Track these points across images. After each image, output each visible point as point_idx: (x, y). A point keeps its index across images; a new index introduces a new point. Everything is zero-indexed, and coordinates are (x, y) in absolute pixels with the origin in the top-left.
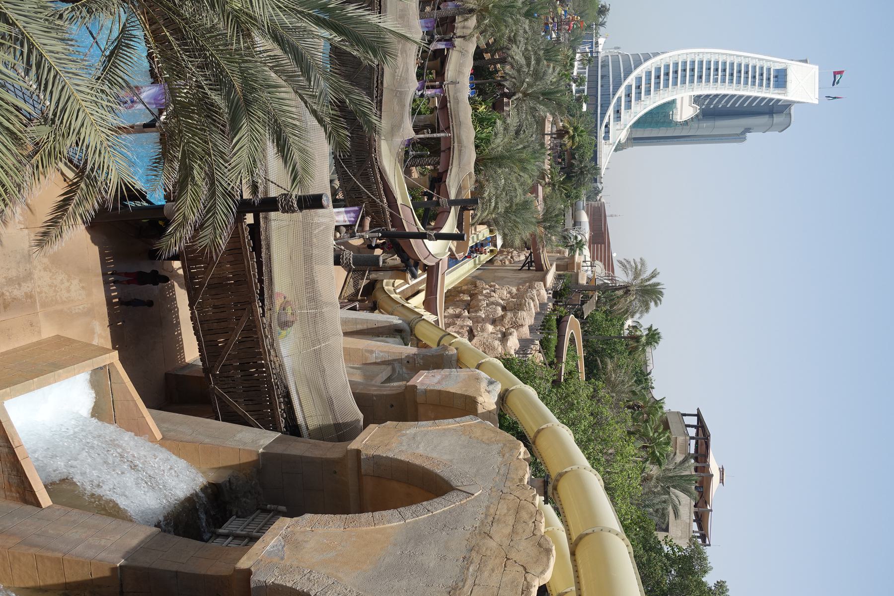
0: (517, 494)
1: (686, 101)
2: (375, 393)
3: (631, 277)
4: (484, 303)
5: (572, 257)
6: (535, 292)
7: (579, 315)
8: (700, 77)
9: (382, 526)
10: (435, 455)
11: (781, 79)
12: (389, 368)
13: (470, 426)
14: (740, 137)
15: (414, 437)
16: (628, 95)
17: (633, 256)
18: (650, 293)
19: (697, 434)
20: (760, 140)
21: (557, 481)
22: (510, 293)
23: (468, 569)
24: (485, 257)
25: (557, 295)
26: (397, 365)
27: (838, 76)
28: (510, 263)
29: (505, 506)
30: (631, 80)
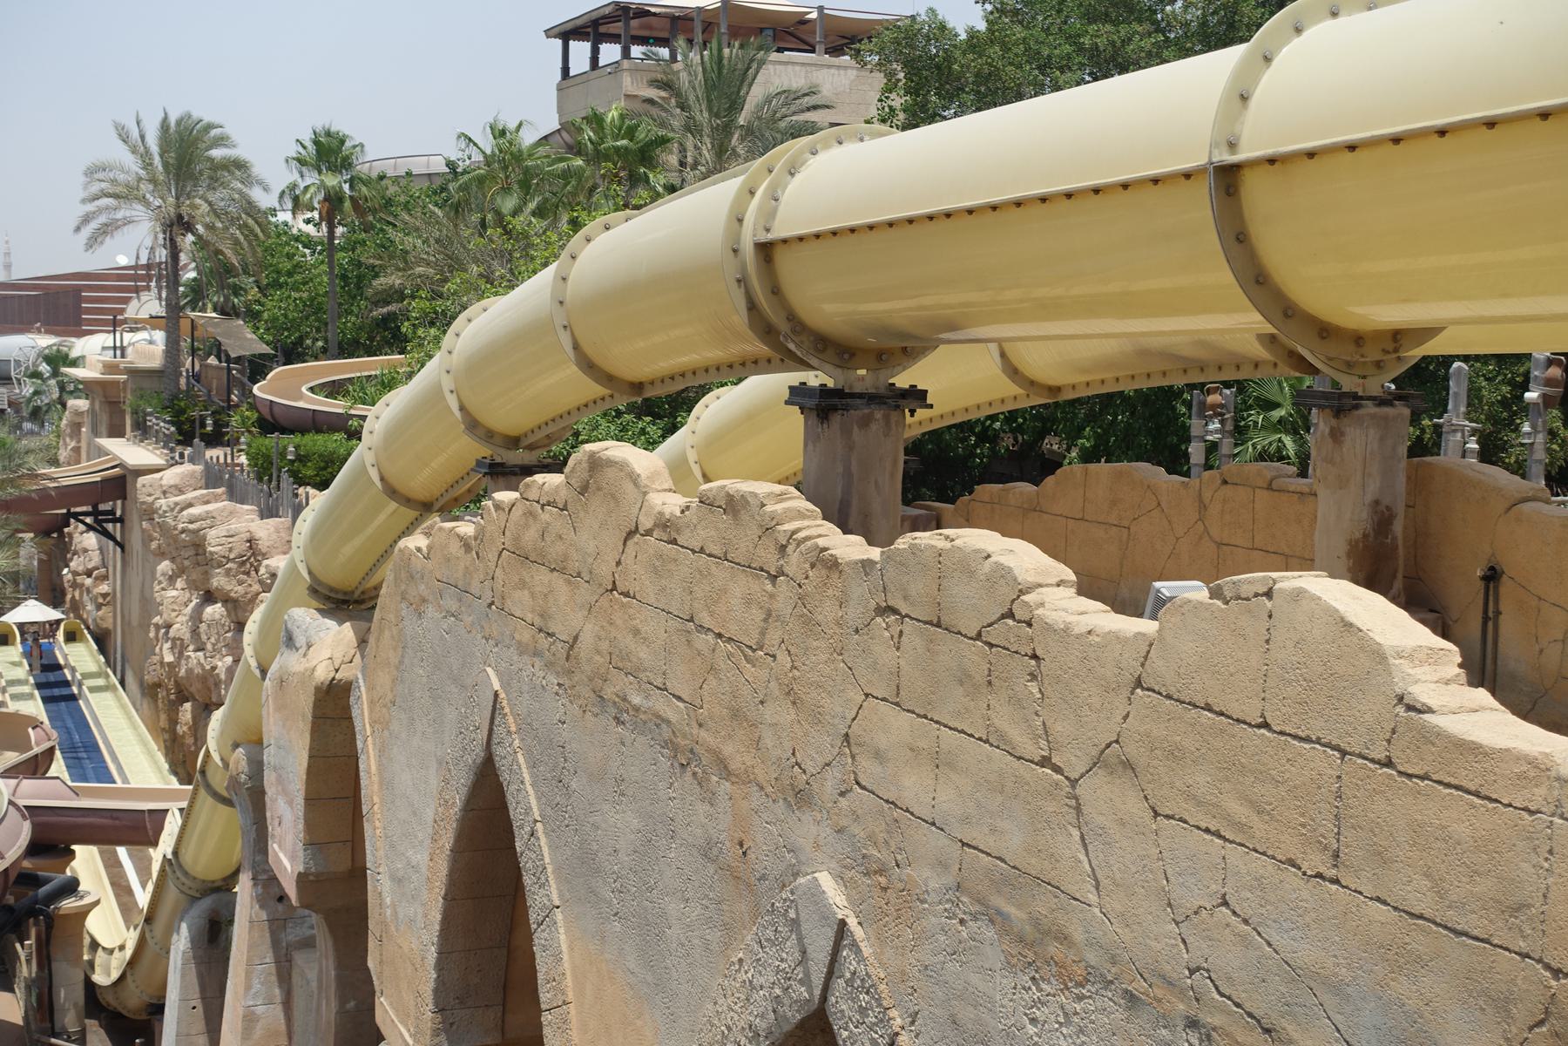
0: (492, 556)
2: (334, 1005)
3: (138, 211)
4: (194, 657)
5: (87, 388)
6: (163, 503)
7: (257, 368)
9: (569, 981)
10: (429, 814)
12: (299, 958)
13: (372, 702)
15: (398, 881)
17: (70, 199)
18: (187, 156)
19: (614, 38)
21: (489, 436)
22: (172, 580)
23: (637, 709)
24: (80, 658)
25: (189, 431)
26: (292, 935)
28: (105, 578)
29: (518, 594)
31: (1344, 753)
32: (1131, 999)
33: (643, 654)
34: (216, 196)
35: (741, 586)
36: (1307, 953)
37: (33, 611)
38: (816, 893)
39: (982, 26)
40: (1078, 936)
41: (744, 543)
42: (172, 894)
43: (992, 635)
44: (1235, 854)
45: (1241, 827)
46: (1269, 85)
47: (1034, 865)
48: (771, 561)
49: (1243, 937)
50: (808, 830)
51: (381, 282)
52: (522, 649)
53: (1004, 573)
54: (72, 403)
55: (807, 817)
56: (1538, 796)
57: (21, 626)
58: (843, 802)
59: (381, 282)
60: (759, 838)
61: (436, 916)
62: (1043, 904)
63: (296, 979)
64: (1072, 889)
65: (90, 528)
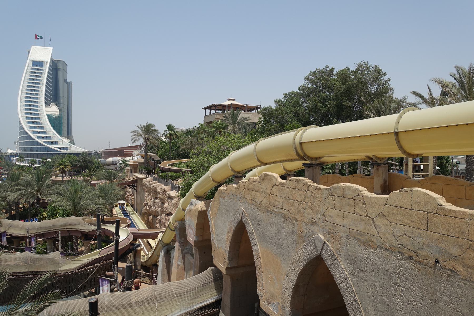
0: (242, 190)
1: (48, 109)
3: (140, 137)
4: (154, 208)
7: (160, 162)
8: (35, 102)
10: (226, 230)
11: (38, 64)
12: (186, 255)
14: (69, 85)
16: (43, 138)
19: (213, 109)
20: (71, 75)
22: (148, 196)
24: (129, 209)
25: (149, 172)
27: (38, 37)
30: (34, 136)
31: (428, 212)
32: (387, 250)
33: (277, 203)
34: (153, 135)
35: (299, 193)
36: (422, 241)
37: (122, 202)
38: (319, 238)
39: (274, 108)
40: (375, 241)
41: (300, 186)
42: (160, 245)
43: (355, 198)
44: (406, 228)
45: (408, 224)
46: (401, 121)
47: (365, 231)
48: (306, 189)
49: (409, 239)
50: (315, 228)
51: (181, 148)
52: (249, 204)
53: (358, 189)
54: (127, 168)
55: (315, 226)
56: (466, 217)
57: (119, 204)
58: (323, 224)
59: (181, 148)
60: (305, 230)
61: (228, 246)
62: (367, 237)
63: (186, 258)
64: (373, 234)
65: (131, 188)
